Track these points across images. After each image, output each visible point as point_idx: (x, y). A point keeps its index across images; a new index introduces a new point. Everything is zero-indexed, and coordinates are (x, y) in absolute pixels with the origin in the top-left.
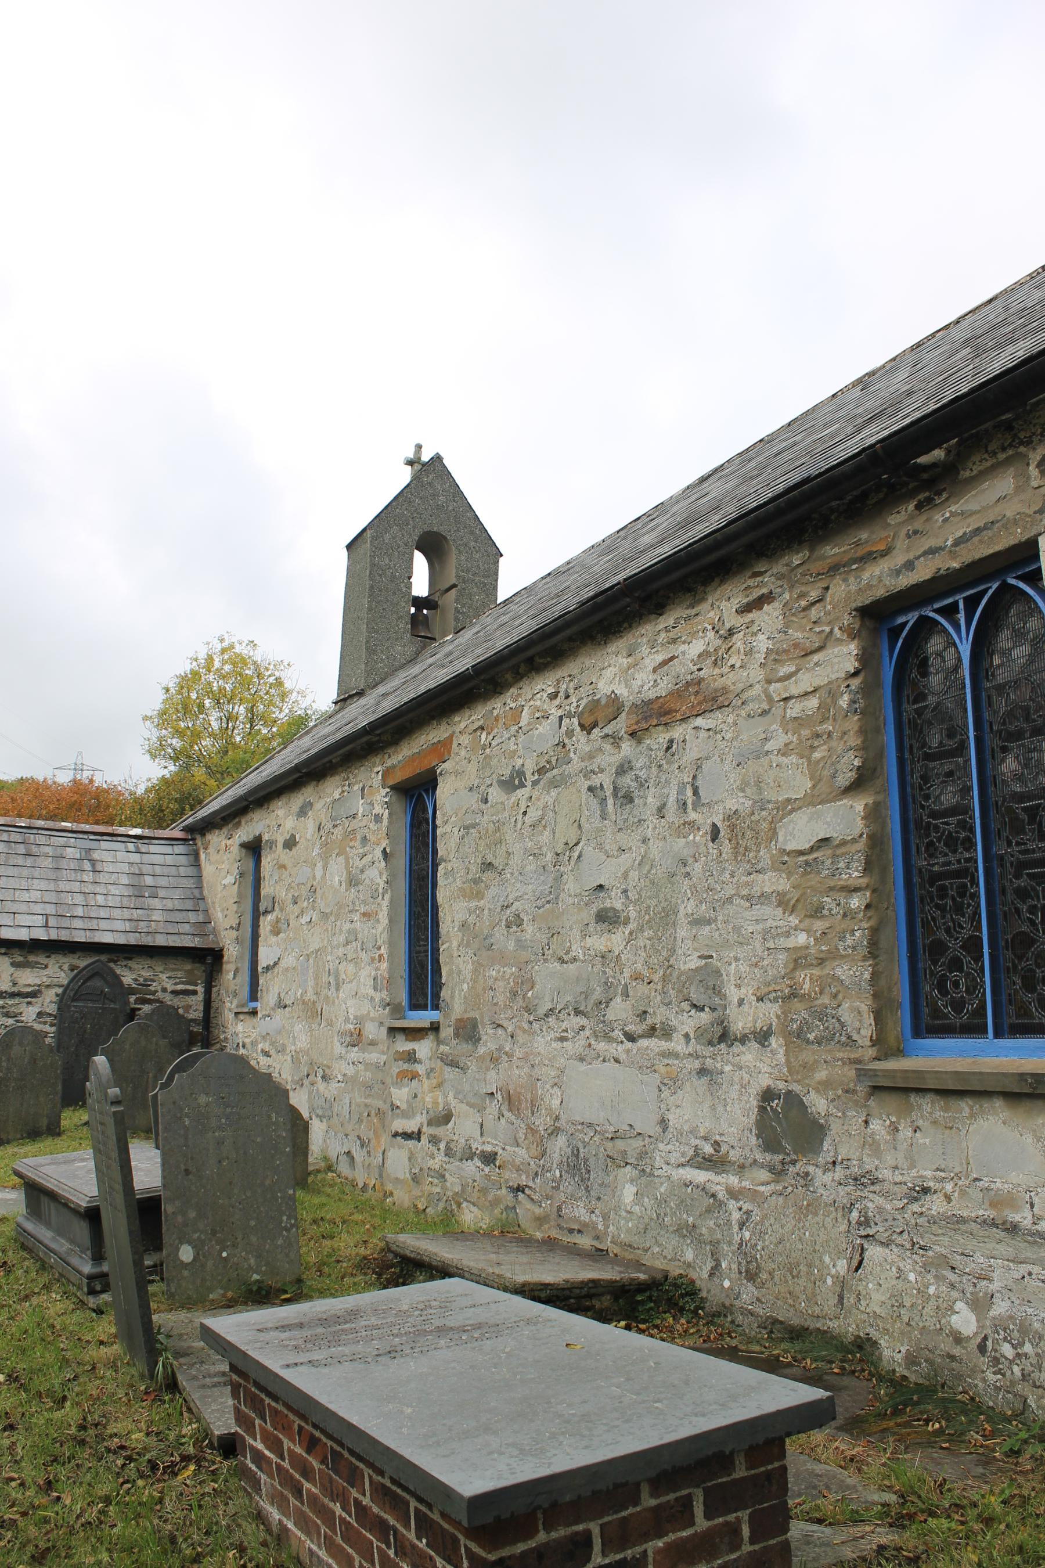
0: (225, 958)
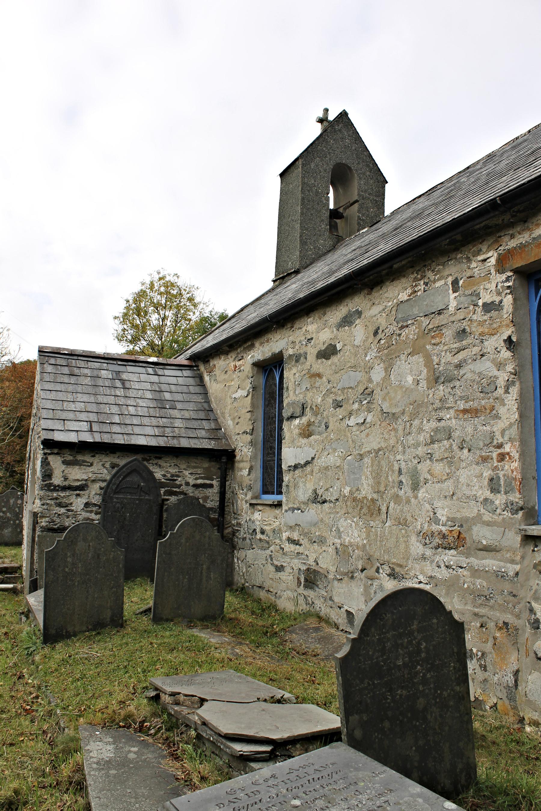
0: (238, 458)
